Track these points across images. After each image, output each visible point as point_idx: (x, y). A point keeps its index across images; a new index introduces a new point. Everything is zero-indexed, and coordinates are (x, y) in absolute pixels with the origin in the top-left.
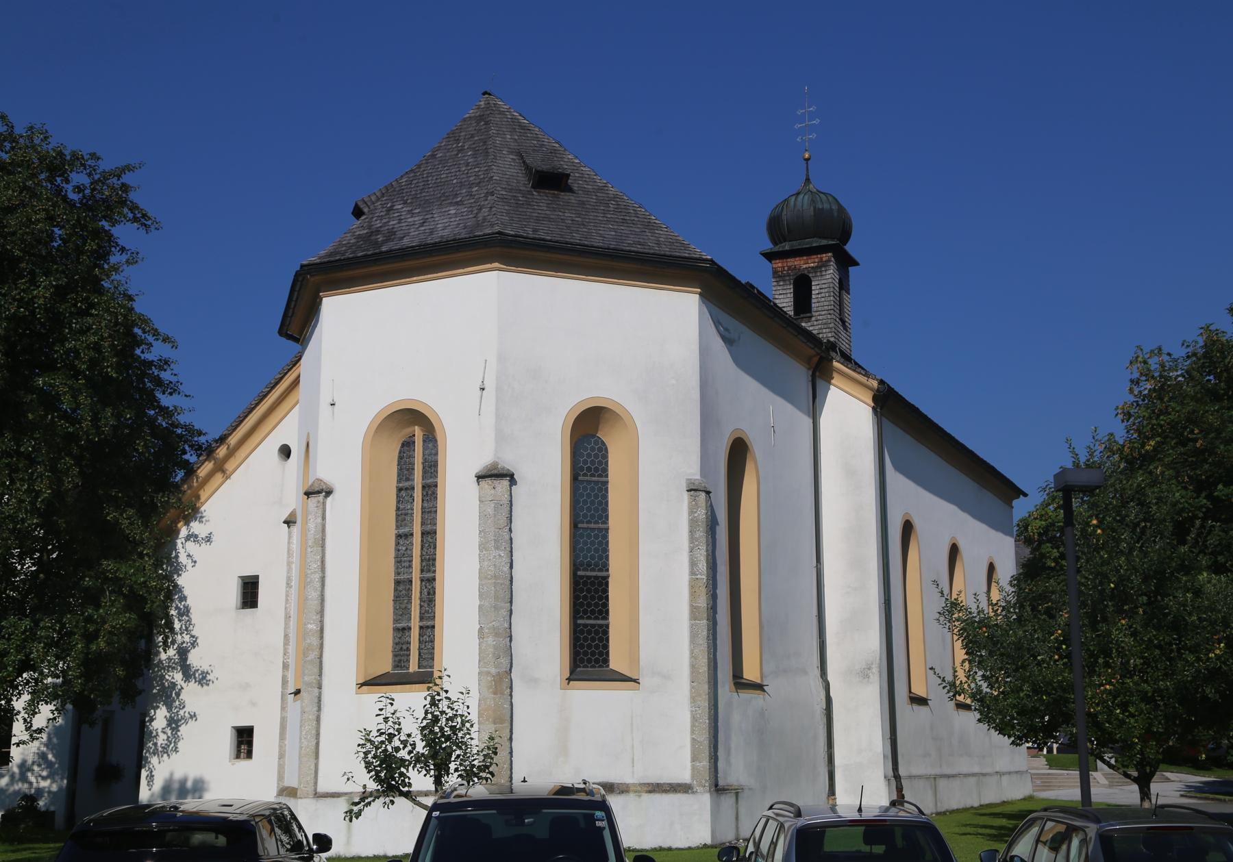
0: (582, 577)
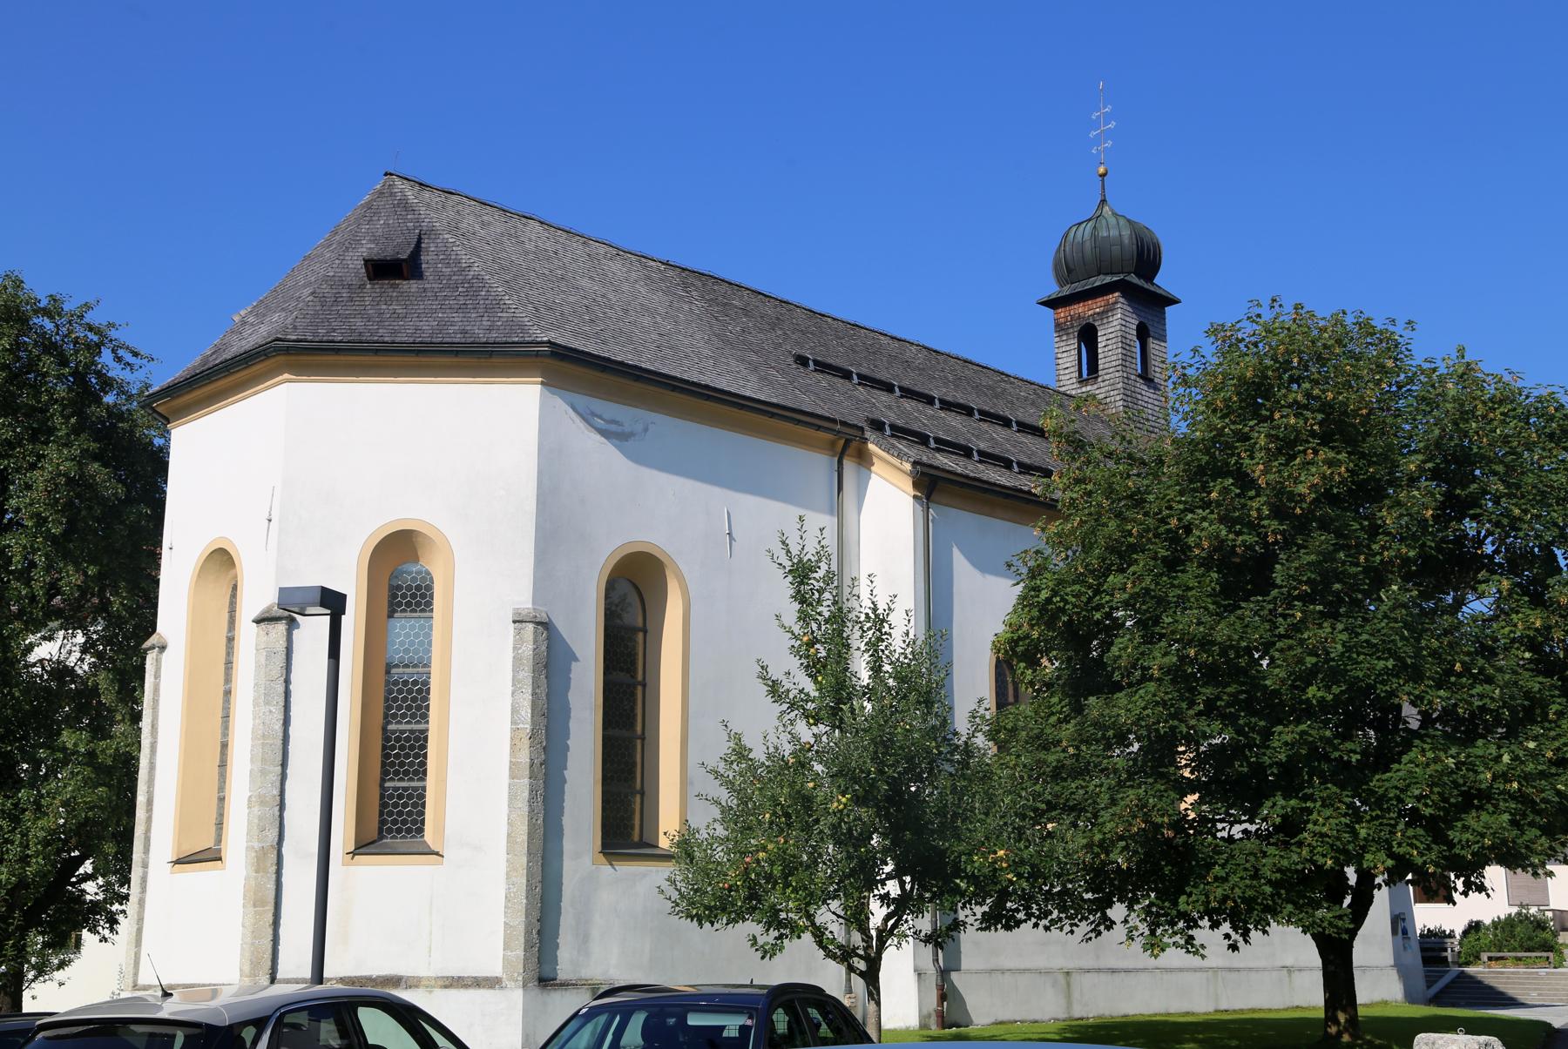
0: (394, 732)
